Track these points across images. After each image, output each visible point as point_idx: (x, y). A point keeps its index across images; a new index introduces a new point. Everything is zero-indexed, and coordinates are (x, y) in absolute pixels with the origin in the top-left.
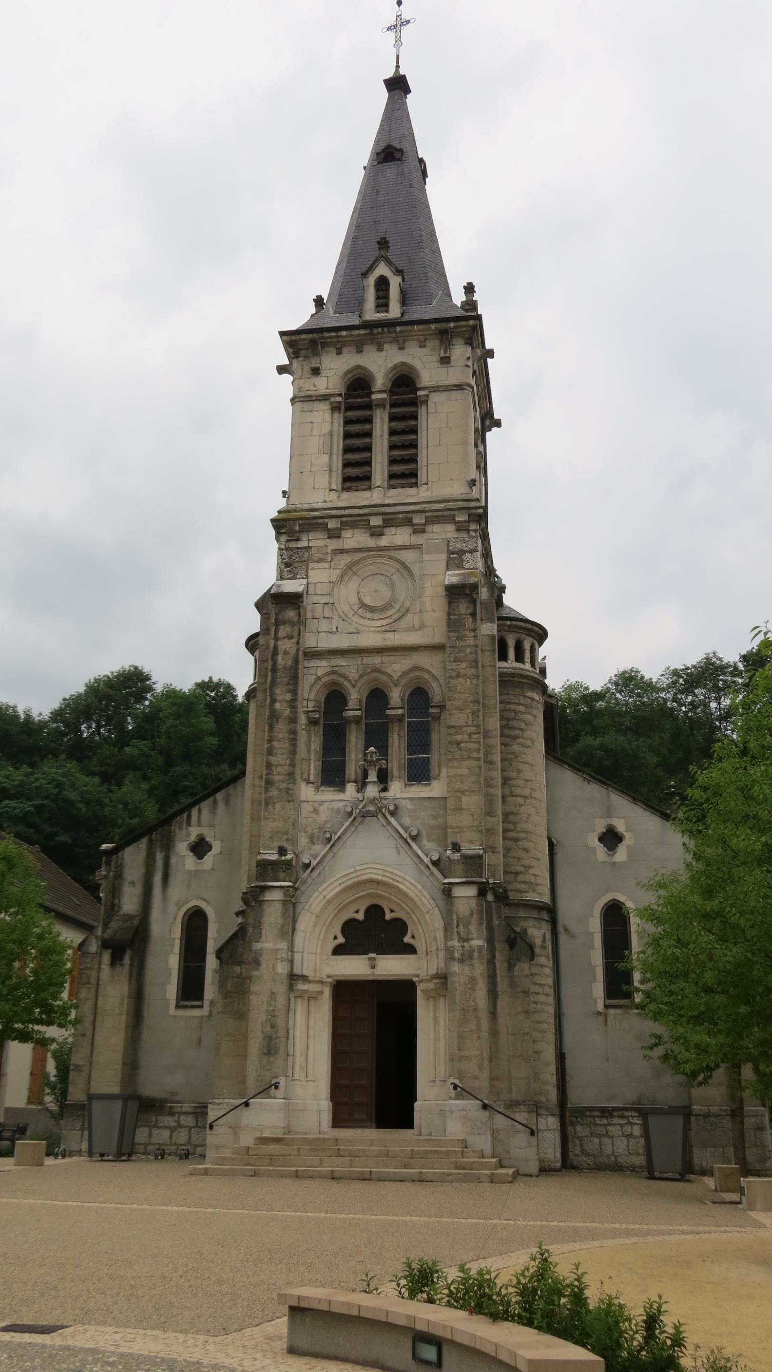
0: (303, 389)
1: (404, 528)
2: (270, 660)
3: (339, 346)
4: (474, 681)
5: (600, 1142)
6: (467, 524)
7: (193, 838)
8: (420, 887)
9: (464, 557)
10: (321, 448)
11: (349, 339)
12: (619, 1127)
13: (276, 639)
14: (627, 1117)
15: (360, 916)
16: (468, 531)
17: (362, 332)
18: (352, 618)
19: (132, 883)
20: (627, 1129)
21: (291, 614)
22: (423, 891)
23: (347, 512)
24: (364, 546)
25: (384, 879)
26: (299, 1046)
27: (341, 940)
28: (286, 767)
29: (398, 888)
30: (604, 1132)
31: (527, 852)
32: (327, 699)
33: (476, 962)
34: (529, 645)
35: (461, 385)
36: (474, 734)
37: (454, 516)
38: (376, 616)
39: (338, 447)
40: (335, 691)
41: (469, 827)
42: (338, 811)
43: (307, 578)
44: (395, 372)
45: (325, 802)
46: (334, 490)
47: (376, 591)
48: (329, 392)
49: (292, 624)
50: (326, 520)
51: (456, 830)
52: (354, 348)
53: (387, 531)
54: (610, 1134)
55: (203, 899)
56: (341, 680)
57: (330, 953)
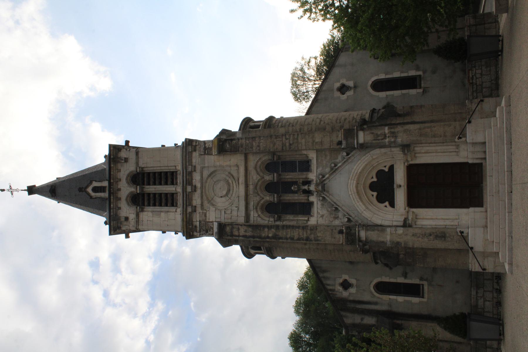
0: (134, 225)
2: (249, 239)
4: (262, 138)
5: (485, 88)
7: (340, 289)
8: (360, 161)
9: (207, 147)
13: (239, 236)
14: (472, 76)
15: (375, 194)
16: (196, 146)
17: (112, 197)
19: (362, 319)
20: (478, 76)
21: (228, 229)
22: (361, 160)
23: (185, 203)
24: (200, 195)
25: (355, 180)
26: (441, 223)
27: (387, 203)
29: (360, 172)
31: (346, 119)
32: (269, 212)
33: (396, 130)
34: (252, 123)
36: (286, 137)
37: (189, 152)
38: (231, 188)
40: (266, 209)
41: (330, 138)
42: (322, 205)
43: (212, 222)
44: (130, 183)
45: (318, 212)
47: (220, 188)
48: (135, 213)
49: (233, 228)
50: (188, 212)
53: (194, 184)
54: (481, 83)
55: (370, 284)
56: (260, 205)
57: (393, 209)
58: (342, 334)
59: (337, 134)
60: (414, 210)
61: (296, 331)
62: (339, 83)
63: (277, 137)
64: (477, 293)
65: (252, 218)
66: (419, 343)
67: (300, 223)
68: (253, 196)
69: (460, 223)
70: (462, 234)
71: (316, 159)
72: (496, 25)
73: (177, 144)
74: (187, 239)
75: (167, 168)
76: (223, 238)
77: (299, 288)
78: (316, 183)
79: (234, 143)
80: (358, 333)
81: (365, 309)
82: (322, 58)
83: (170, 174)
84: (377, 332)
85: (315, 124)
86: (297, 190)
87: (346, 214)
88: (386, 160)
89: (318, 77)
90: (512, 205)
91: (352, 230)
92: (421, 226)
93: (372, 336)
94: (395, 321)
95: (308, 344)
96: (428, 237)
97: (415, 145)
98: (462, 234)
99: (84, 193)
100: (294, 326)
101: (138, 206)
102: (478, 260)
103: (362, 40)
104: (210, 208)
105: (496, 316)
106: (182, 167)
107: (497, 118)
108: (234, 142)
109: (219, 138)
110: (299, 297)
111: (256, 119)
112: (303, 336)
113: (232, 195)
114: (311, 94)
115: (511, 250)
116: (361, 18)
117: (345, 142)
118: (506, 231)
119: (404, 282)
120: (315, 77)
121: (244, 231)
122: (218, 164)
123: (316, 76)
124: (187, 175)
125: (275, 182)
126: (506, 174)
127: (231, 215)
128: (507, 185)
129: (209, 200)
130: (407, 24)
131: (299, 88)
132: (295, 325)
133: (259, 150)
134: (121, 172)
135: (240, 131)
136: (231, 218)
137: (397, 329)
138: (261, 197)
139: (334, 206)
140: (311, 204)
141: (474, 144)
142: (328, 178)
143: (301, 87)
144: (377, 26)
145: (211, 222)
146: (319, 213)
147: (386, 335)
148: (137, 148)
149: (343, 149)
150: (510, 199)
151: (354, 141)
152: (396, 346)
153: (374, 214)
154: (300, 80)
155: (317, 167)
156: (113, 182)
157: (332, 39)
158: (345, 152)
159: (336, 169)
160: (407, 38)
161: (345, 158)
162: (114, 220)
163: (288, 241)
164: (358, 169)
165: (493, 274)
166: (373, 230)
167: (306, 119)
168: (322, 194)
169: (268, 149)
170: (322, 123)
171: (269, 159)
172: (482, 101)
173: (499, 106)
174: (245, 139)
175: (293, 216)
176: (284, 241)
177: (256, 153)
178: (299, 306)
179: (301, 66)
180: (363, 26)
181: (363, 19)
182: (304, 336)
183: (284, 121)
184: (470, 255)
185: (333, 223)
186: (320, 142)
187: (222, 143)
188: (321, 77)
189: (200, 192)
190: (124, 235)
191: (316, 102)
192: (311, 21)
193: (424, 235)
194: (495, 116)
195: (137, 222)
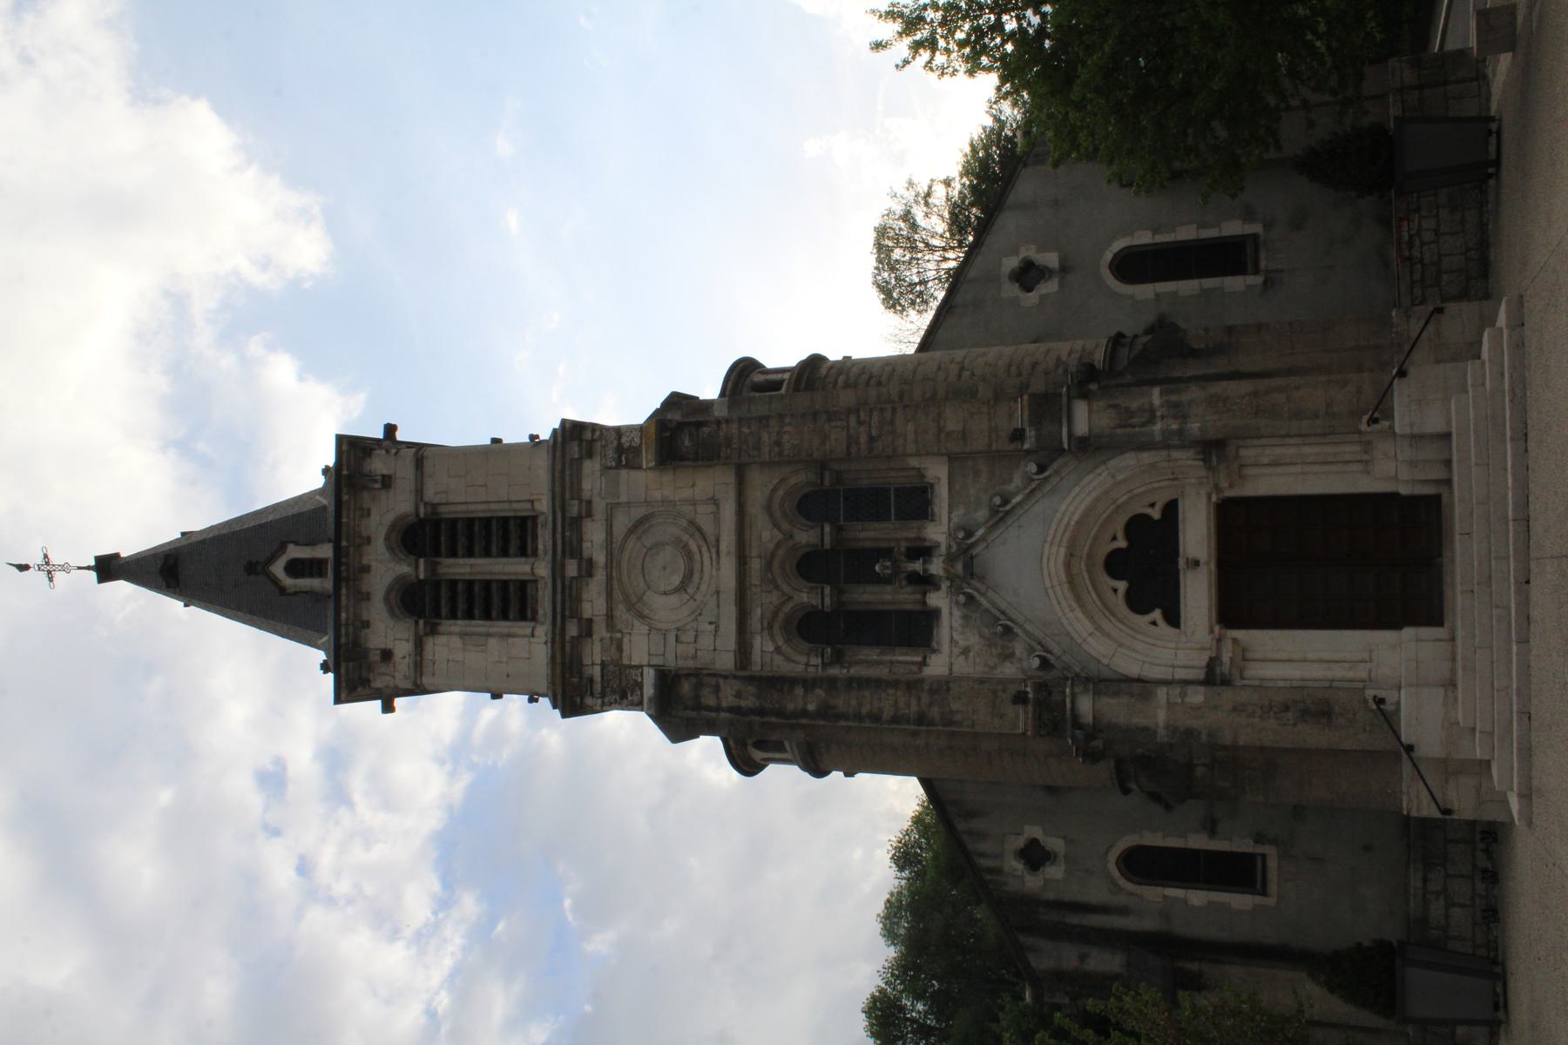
1: (584, 529)
4: (787, 420)
6: (584, 443)
7: (1018, 866)
8: (1077, 489)
10: (479, 649)
11: (351, 610)
12: (1425, 248)
13: (718, 709)
14: (1411, 237)
15: (1122, 586)
16: (593, 441)
17: (344, 591)
20: (1428, 236)
21: (686, 688)
22: (1082, 484)
25: (1064, 544)
26: (1318, 672)
27: (1157, 614)
29: (1078, 523)
33: (1185, 398)
36: (859, 417)
37: (572, 460)
38: (697, 567)
39: (482, 626)
42: (966, 617)
43: (642, 666)
47: (665, 568)
48: (412, 638)
49: (699, 686)
50: (568, 638)
53: (586, 554)
57: (1178, 630)
58: (1023, 999)
60: (1239, 634)
64: (1425, 880)
65: (756, 657)
69: (1373, 675)
70: (1382, 706)
71: (949, 484)
73: (537, 437)
74: (564, 715)
75: (506, 506)
77: (895, 863)
78: (948, 554)
82: (968, 183)
84: (1127, 995)
85: (946, 380)
86: (892, 574)
88: (1156, 485)
92: (1257, 683)
98: (1382, 706)
100: (880, 976)
101: (420, 618)
102: (1429, 783)
103: (1085, 133)
104: (632, 626)
108: (706, 430)
109: (661, 418)
110: (896, 890)
111: (770, 362)
112: (906, 1004)
113: (698, 588)
115: (1527, 752)
116: (1080, 66)
117: (1033, 433)
118: (1511, 700)
120: (946, 238)
122: (658, 495)
123: (948, 235)
126: (1511, 527)
133: (780, 454)
134: (373, 517)
135: (724, 399)
138: (784, 594)
139: (1000, 623)
140: (931, 616)
141: (1416, 438)
142: (983, 539)
143: (903, 268)
145: (635, 666)
149: (1028, 452)
150: (1525, 602)
153: (1120, 645)
154: (901, 247)
156: (347, 547)
159: (1008, 513)
160: (1215, 124)
161: (1033, 480)
165: (1472, 824)
166: (1116, 694)
167: (919, 364)
168: (964, 585)
170: (966, 374)
172: (1440, 311)
175: (878, 651)
176: (851, 724)
177: (770, 464)
179: (906, 205)
182: (909, 1004)
189: (605, 578)
190: (378, 704)
191: (947, 312)
192: (933, 76)
194: (1479, 357)
195: (419, 665)
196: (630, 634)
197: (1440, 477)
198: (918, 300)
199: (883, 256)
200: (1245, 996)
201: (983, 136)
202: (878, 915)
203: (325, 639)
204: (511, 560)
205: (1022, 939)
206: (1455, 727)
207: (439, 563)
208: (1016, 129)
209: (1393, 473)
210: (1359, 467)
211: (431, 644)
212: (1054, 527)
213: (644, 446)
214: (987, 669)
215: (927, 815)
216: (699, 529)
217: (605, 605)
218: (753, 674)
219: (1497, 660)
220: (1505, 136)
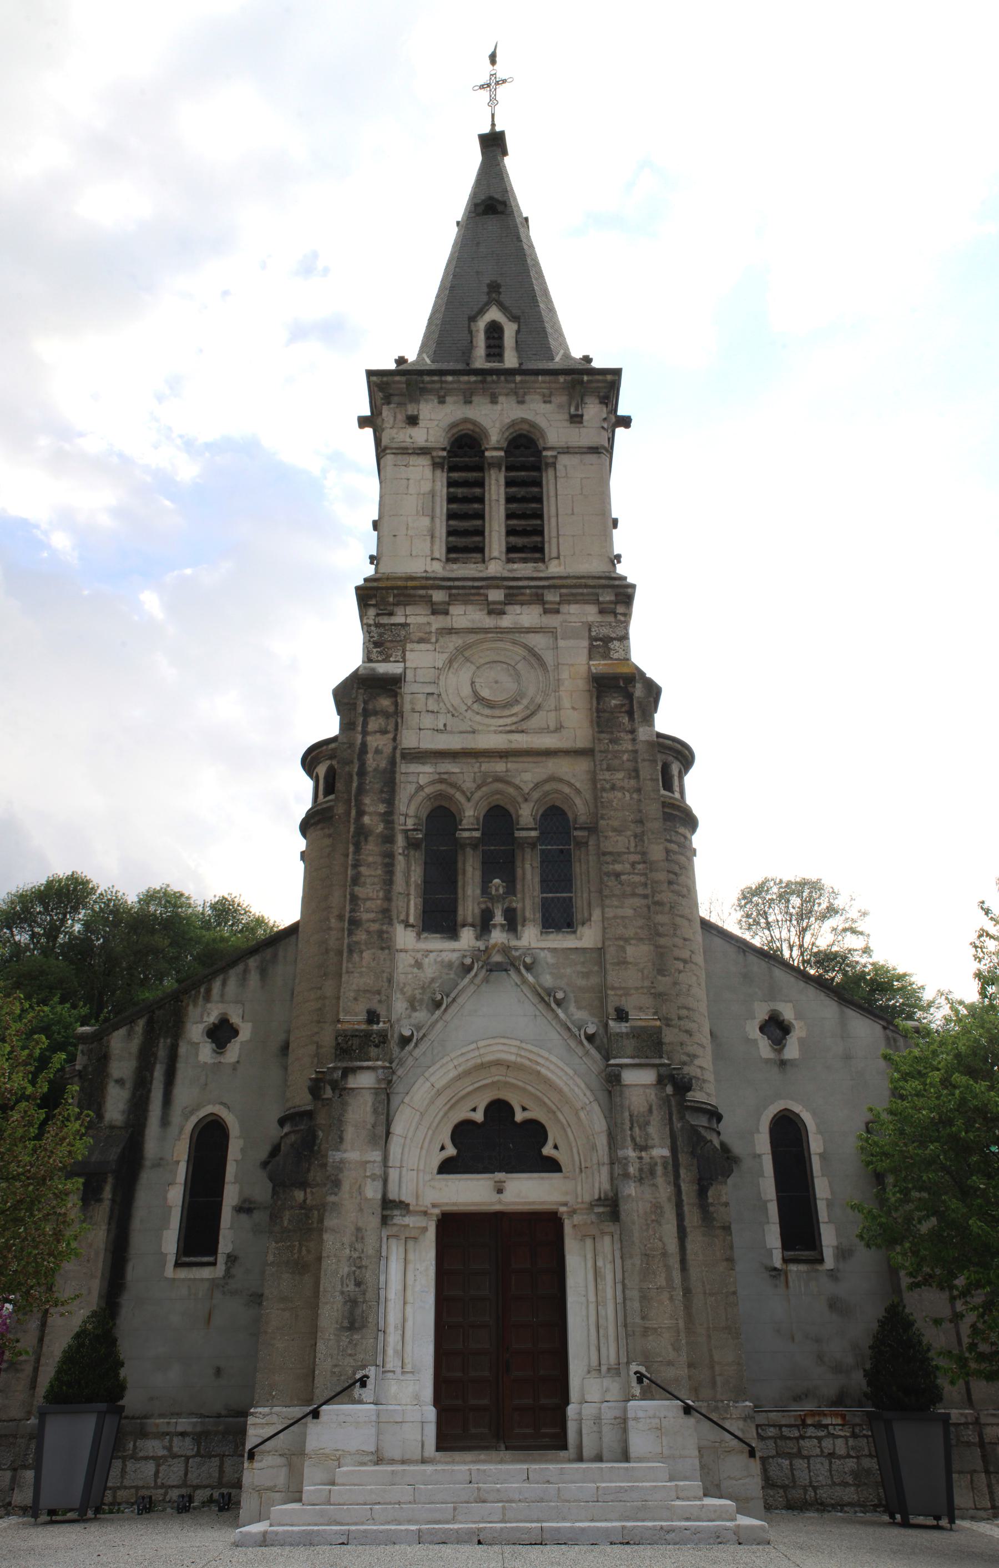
0: (395, 440)
1: (533, 606)
2: (356, 761)
3: (442, 393)
4: (635, 796)
5: (791, 1464)
6: (613, 606)
7: (212, 1018)
8: (571, 1072)
9: (611, 646)
10: (420, 508)
11: (455, 386)
13: (365, 733)
14: (826, 1426)
15: (479, 1117)
16: (615, 614)
17: (473, 378)
18: (466, 714)
19: (120, 1082)
20: (827, 1444)
21: (385, 703)
22: (576, 1078)
23: (457, 583)
24: (480, 625)
25: (519, 1059)
26: (393, 1318)
27: (451, 1151)
28: (379, 902)
29: (539, 1073)
30: (795, 1450)
31: (691, 1035)
33: (660, 1180)
34: (678, 770)
35: (597, 448)
36: (639, 863)
37: (597, 595)
38: (497, 712)
40: (440, 807)
41: (637, 988)
42: (450, 965)
43: (404, 661)
44: (511, 430)
45: (431, 952)
46: (438, 559)
47: (496, 682)
48: (429, 445)
49: (387, 715)
50: (430, 592)
51: (620, 992)
52: (461, 397)
53: (509, 608)
54: (805, 1453)
55: (222, 1103)
57: (435, 1171)
58: (82, 1025)
59: (648, 1008)
60: (431, 1234)
61: (94, 894)
62: (793, 1017)
63: (639, 837)
64: (183, 1434)
65: (414, 768)
66: (38, 1254)
67: (398, 904)
68: (475, 773)
69: (390, 1375)
70: (358, 1384)
71: (576, 948)
72: (985, 1509)
73: (619, 562)
74: (358, 589)
75: (554, 534)
76: (359, 688)
77: (218, 901)
78: (510, 947)
79: (620, 719)
80: (80, 1071)
81: (149, 1091)
82: (867, 970)
83: (537, 542)
84: (81, 1126)
85: (674, 946)
86: (491, 894)
87: (423, 1031)
88: (575, 1150)
89: (811, 955)
90: (441, 1545)
91: (376, 1050)
92: (384, 1254)
93: (68, 1110)
94: (110, 1180)
95: (53, 931)
96: (352, 1278)
97: (616, 1237)
98: (358, 1384)
99: (484, 298)
100: (109, 888)
101: (449, 452)
102: (281, 1435)
103: (919, 1087)
104: (442, 652)
105: (109, 1497)
106: (556, 575)
107: (700, 1499)
108: (626, 720)
109: (637, 678)
110: (192, 902)
111: (689, 779)
112: (79, 913)
113: (478, 713)
114: (762, 935)
115: (308, 1541)
116: (988, 1083)
117: (624, 1030)
118: (362, 1524)
119: (224, 1203)
120: (812, 948)
121: (380, 747)
122: (565, 675)
123: (815, 950)
124: (533, 590)
125: (513, 834)
126: (534, 1525)
127: (424, 709)
128: (502, 1529)
129: (466, 649)
130: (975, 1224)
131: (780, 901)
132: (112, 892)
133: (603, 789)
134: (543, 406)
135: (655, 736)
136: (413, 711)
137: (84, 1184)
138: (472, 793)
139: (445, 998)
140: (451, 930)
141: (623, 1423)
142: (524, 981)
143: (782, 906)
144: (963, 1133)
145: (405, 655)
146: (426, 957)
147: (70, 1152)
148: (609, 450)
149: (606, 1025)
150: (460, 1539)
151: (628, 1057)
152: (31, 1184)
153: (422, 1115)
154: (802, 905)
155: (555, 948)
156: (514, 382)
157: (924, 1003)
158: (598, 1028)
159: (548, 1005)
160: (934, 1220)
161: (580, 1030)
162: (408, 383)
163: (350, 868)
164: (548, 1068)
165: (238, 1485)
166: (375, 1111)
167: (689, 920)
168: (481, 963)
169: (604, 812)
170: (680, 965)
171: (576, 815)
172: (752, 1454)
173: (737, 1508)
174: (632, 751)
175: (419, 882)
176: (350, 857)
177: (594, 781)
178: (168, 901)
179: (843, 909)
180: (961, 1089)
181: (983, 1089)
182: (81, 916)
183: (682, 859)
184: (297, 1409)
185: (399, 996)
186: (626, 958)
187: (620, 687)
188: (811, 966)
189: (487, 626)
190: (367, 412)
191: (739, 947)
192: (973, 937)
193: (358, 1264)
194: (705, 1495)
195: (404, 451)
196: (435, 649)
197: (584, 1450)
198: (751, 921)
199: (793, 887)
200: (74, 1245)
201: (914, 986)
202: (168, 886)
203: (428, 361)
204: (503, 538)
205: (141, 1023)
206: (336, 1463)
207: (500, 470)
208: (921, 1023)
209: (588, 1398)
210: (594, 1362)
211: (425, 464)
212: (535, 1049)
213: (610, 662)
214: (402, 985)
215: (265, 931)
216: (533, 714)
217: (463, 626)
218: (398, 765)
219: (402, 1508)
220: (936, 1534)
